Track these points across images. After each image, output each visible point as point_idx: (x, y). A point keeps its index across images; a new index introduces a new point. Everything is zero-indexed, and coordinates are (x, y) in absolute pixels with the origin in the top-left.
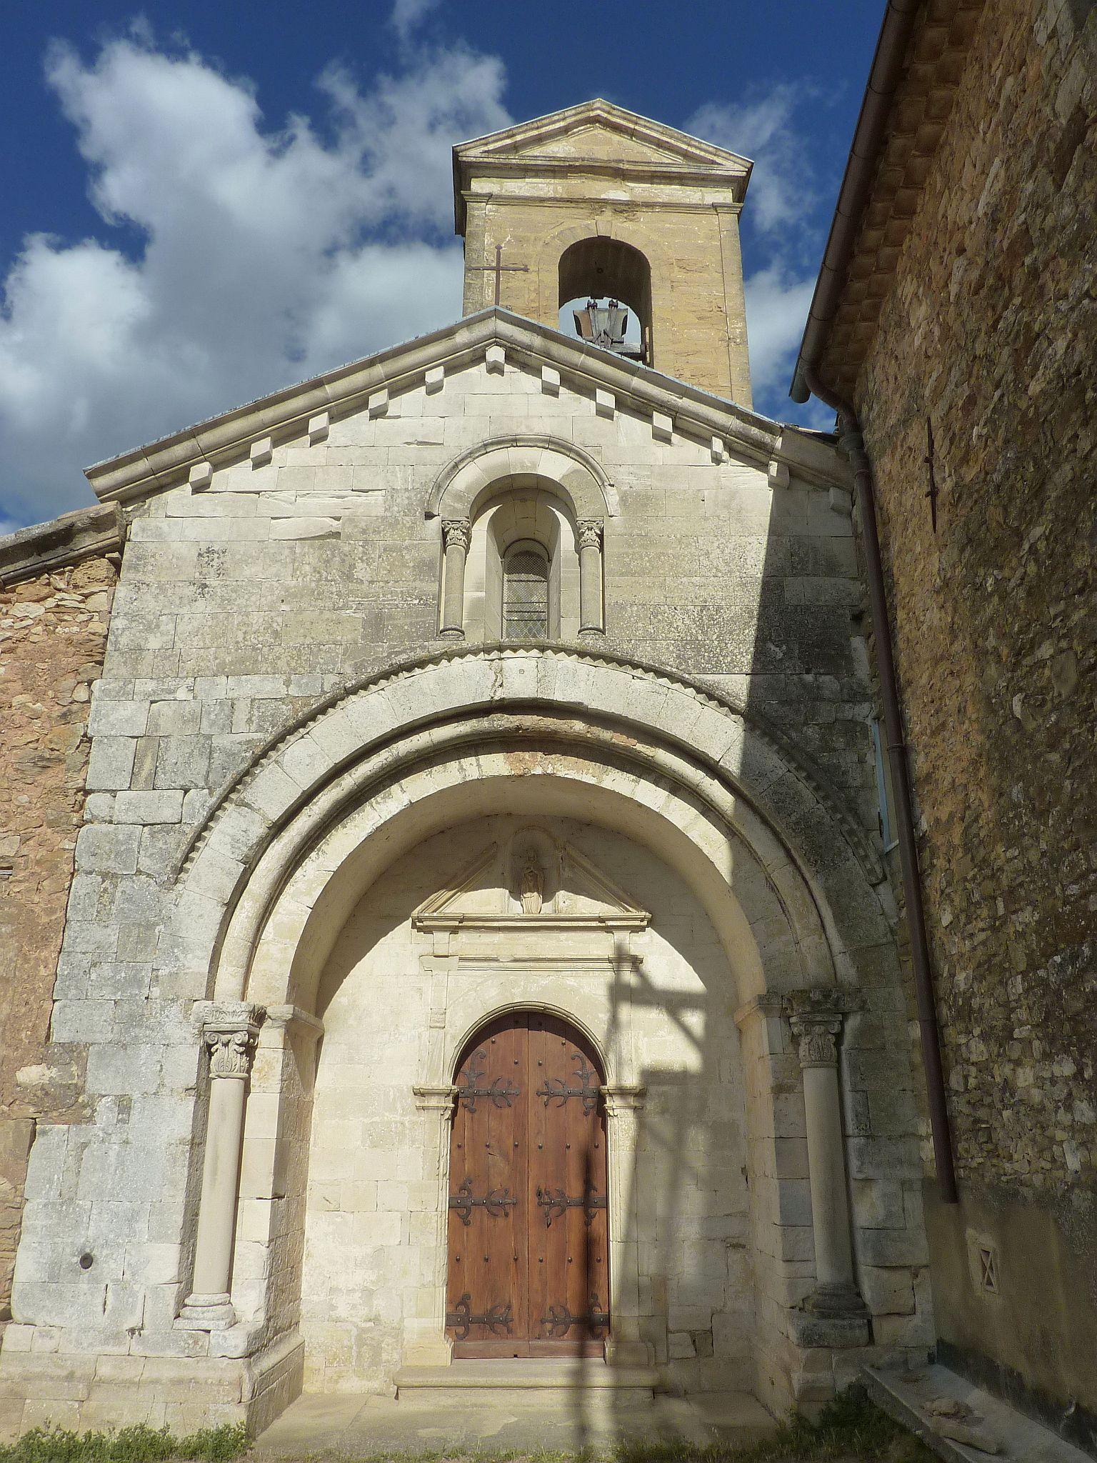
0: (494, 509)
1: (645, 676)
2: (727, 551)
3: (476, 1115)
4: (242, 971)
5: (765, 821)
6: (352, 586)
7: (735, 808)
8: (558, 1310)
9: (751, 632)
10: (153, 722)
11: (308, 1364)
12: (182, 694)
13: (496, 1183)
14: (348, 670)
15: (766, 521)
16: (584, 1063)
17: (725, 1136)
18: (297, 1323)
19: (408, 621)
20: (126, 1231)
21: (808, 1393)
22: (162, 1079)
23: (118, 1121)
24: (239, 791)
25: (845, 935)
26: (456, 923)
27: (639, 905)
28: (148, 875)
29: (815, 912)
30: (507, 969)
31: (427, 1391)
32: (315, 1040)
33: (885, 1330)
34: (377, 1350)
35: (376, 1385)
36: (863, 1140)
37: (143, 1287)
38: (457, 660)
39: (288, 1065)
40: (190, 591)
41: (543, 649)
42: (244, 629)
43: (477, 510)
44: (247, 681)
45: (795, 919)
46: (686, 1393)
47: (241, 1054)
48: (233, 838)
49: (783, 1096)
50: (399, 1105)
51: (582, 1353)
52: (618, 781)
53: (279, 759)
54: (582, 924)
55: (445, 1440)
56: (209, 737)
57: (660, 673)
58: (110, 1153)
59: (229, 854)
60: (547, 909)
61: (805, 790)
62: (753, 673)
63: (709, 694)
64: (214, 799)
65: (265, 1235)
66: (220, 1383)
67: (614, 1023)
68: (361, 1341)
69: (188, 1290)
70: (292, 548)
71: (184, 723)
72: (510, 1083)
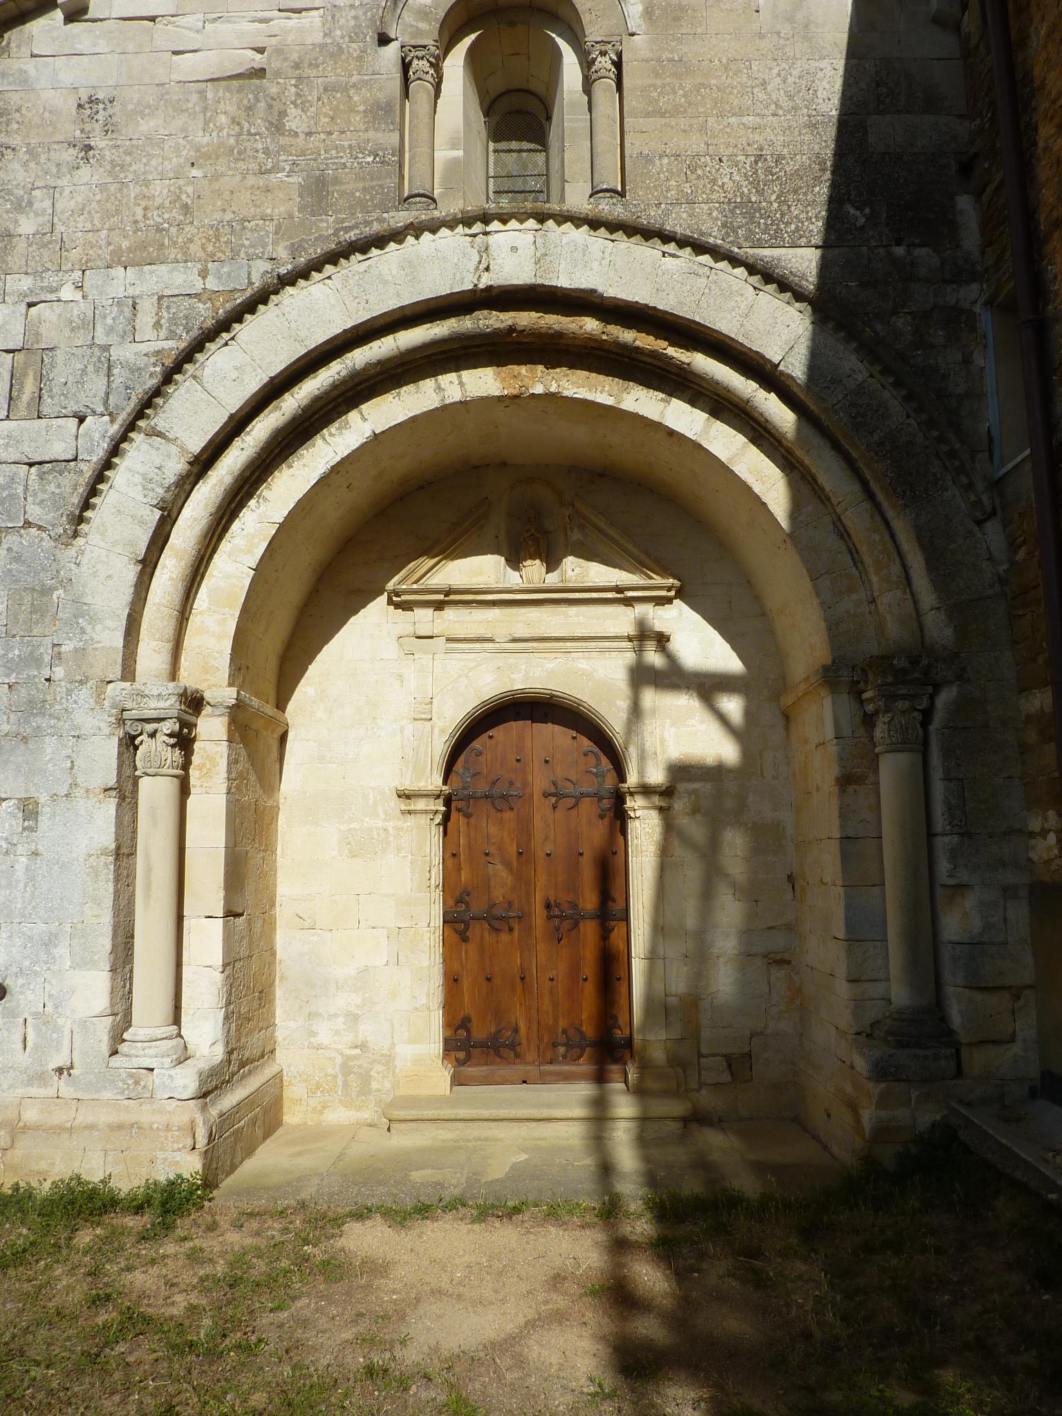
0: (473, 37)
1: (680, 253)
2: (790, 80)
3: (472, 820)
4: (169, 646)
5: (836, 446)
6: (283, 141)
7: (799, 430)
8: (572, 1032)
9: (822, 191)
10: (31, 330)
11: (287, 1094)
12: (67, 293)
13: (498, 894)
14: (282, 253)
15: (843, 38)
16: (598, 759)
17: (767, 839)
18: (272, 1052)
19: (360, 185)
20: (44, 957)
21: (882, 1132)
22: (74, 777)
23: (24, 829)
24: (148, 417)
25: (941, 582)
26: (441, 597)
27: (664, 571)
28: (40, 528)
29: (898, 561)
30: (504, 651)
31: (422, 1125)
32: (277, 735)
33: (977, 1060)
34: (365, 1079)
35: (366, 1115)
36: (956, 839)
37: (69, 1022)
38: (427, 236)
39: (237, 762)
40: (69, 155)
41: (542, 218)
42: (143, 204)
43: (450, 35)
44: (151, 272)
45: (871, 570)
46: (720, 1120)
47: (173, 746)
48: (144, 476)
49: (851, 789)
50: (380, 810)
51: (600, 1078)
52: (641, 401)
53: (197, 373)
54: (595, 595)
55: (442, 1185)
56: (106, 348)
57: (700, 248)
58: (17, 867)
59: (140, 497)
60: (553, 579)
61: (893, 401)
62: (825, 246)
63: (767, 275)
64: (116, 427)
65: (217, 959)
66: (168, 1128)
67: (636, 711)
68: (346, 1069)
69: (127, 1022)
70: (202, 93)
71: (72, 330)
72: (511, 783)
